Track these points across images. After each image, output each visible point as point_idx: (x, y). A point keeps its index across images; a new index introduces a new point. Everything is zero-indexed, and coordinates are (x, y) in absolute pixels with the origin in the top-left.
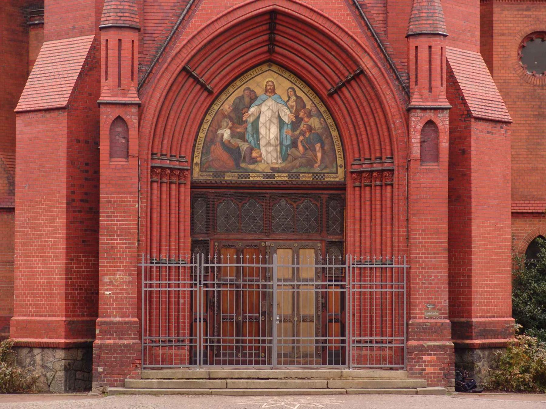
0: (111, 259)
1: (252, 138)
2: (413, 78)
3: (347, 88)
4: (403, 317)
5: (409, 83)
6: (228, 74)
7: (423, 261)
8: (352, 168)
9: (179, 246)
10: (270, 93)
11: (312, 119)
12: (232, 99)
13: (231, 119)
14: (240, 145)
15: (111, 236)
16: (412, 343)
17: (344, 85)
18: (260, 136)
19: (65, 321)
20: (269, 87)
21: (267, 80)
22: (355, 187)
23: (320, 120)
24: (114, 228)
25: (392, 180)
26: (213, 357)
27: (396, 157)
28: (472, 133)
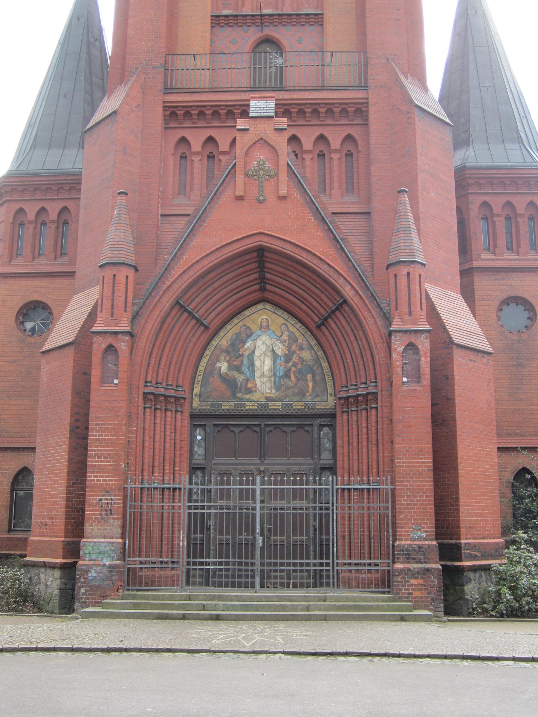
0: (98, 480)
1: (247, 370)
2: (393, 304)
3: (332, 319)
4: (388, 539)
5: (390, 309)
6: (223, 310)
7: (408, 482)
8: (339, 394)
9: (174, 470)
10: (264, 329)
11: (303, 352)
12: (230, 335)
13: (228, 353)
14: (236, 377)
15: (98, 458)
16: (398, 566)
17: (329, 316)
18: (255, 369)
19: (63, 542)
20: (263, 324)
21: (261, 318)
22: (343, 412)
23: (311, 353)
24: (101, 450)
25: (377, 403)
26: (209, 578)
27: (379, 380)
28: (454, 359)
